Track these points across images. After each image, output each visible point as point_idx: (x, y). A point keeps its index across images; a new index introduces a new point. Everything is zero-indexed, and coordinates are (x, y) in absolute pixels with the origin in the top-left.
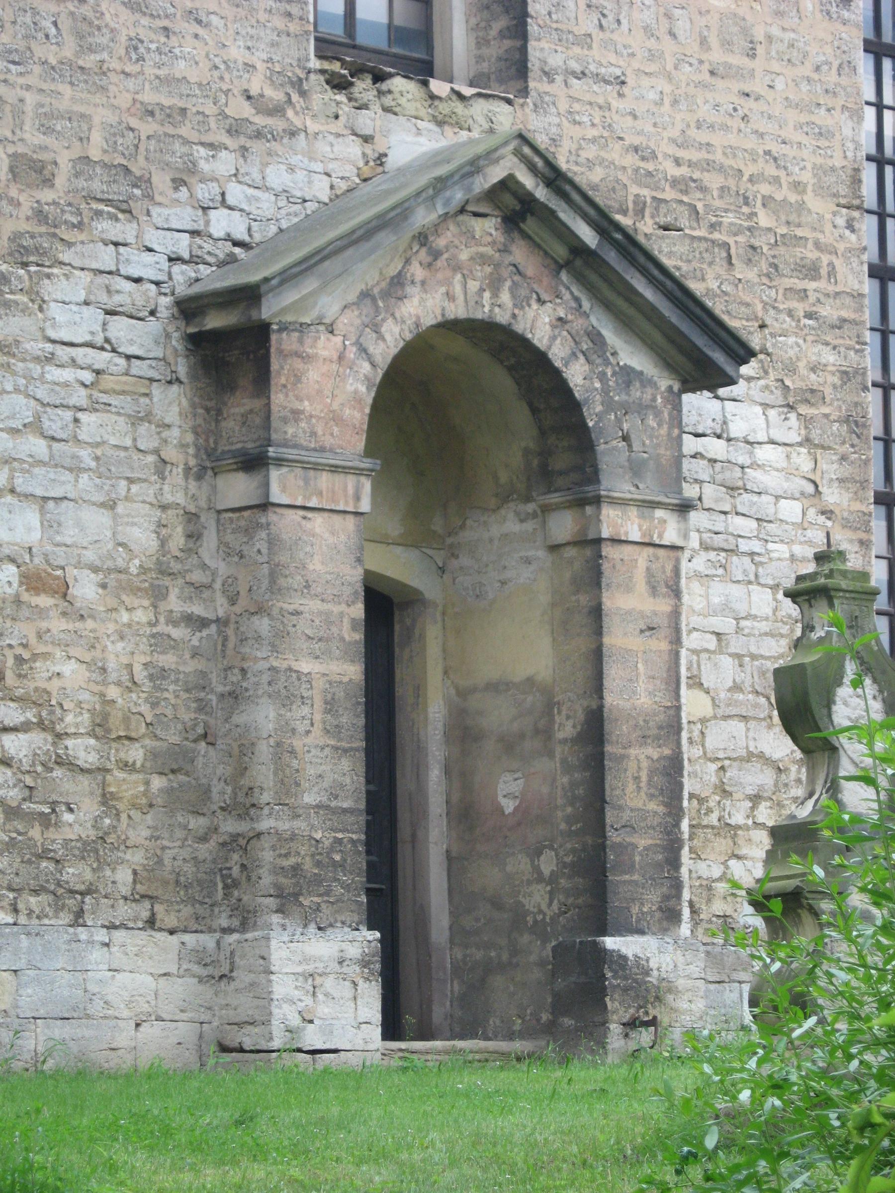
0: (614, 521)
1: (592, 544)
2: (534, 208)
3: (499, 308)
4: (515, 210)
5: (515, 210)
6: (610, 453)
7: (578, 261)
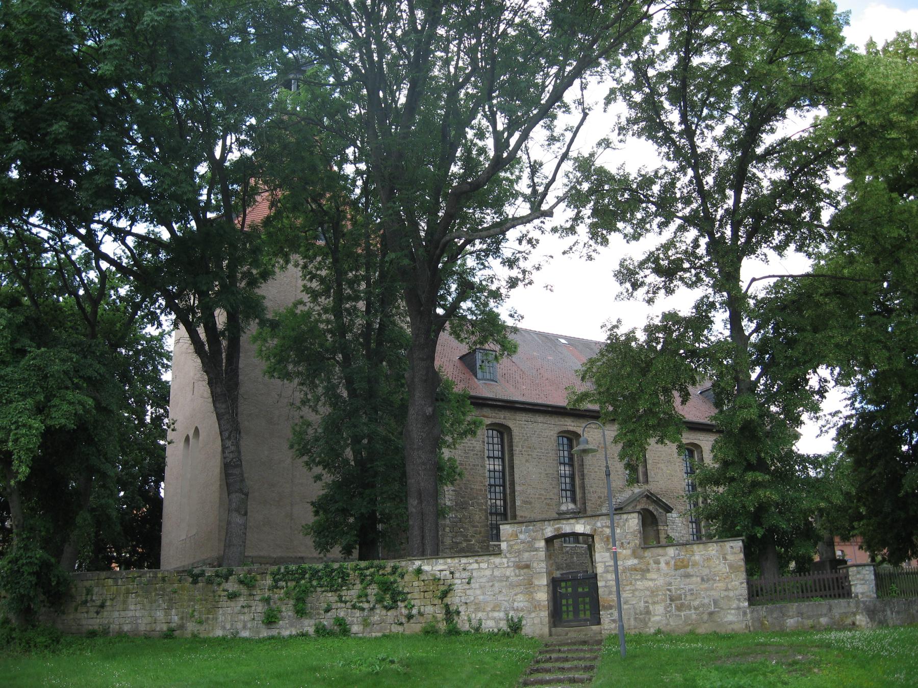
0: (660, 527)
1: (658, 530)
2: (651, 497)
3: (647, 507)
4: (647, 497)
5: (647, 497)
6: (659, 520)
7: (654, 502)
